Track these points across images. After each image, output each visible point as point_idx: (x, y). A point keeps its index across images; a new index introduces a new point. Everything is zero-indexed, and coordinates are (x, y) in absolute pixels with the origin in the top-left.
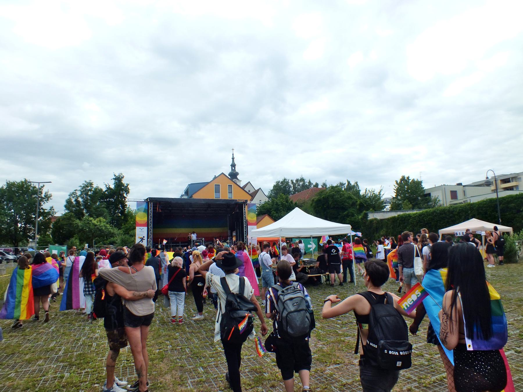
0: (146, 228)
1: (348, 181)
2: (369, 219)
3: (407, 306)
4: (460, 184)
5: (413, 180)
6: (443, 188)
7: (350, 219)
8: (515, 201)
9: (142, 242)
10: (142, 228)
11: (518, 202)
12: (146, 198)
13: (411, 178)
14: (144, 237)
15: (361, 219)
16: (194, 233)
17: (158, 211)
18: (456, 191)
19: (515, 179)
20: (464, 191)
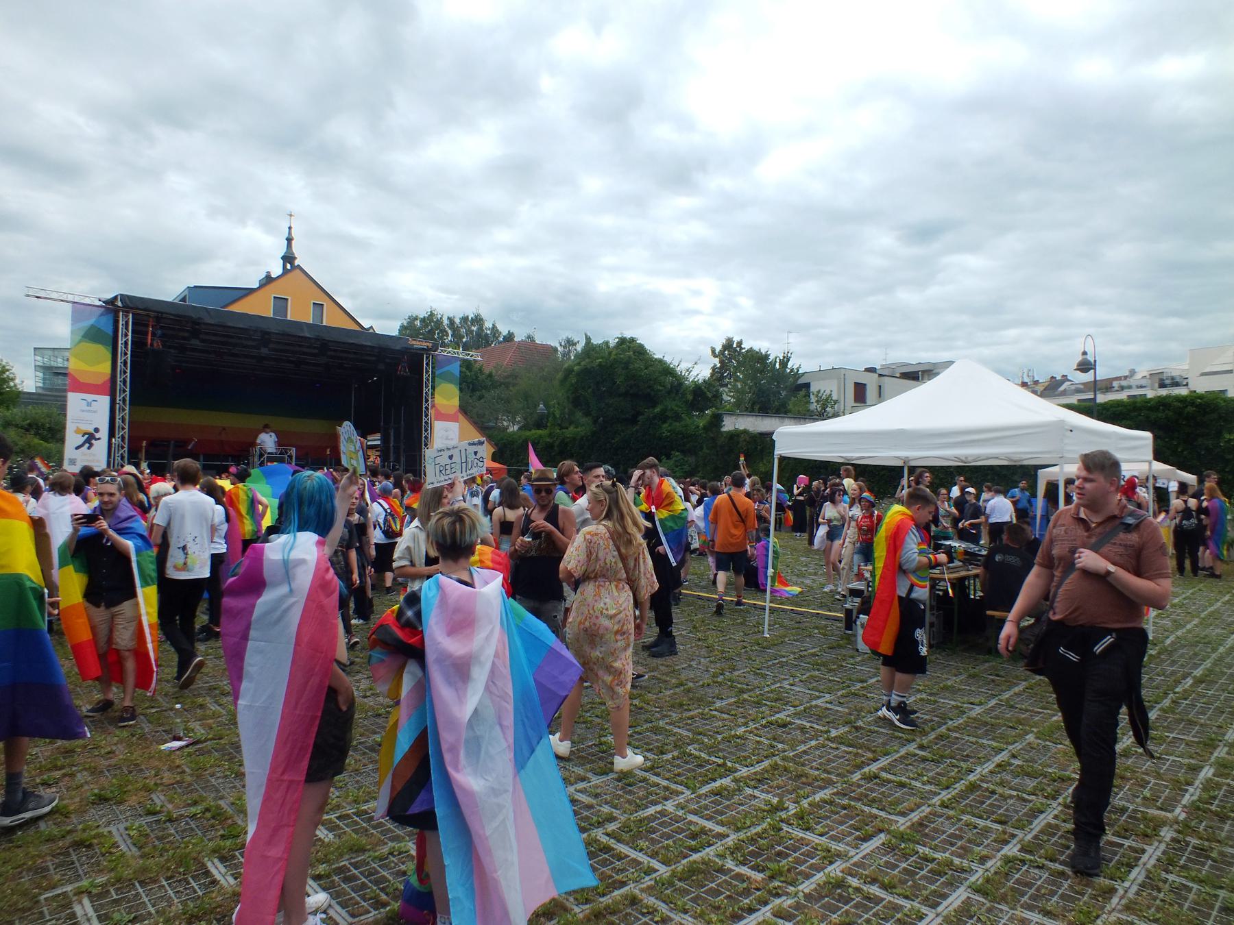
0: (105, 401)
1: (586, 335)
2: (724, 429)
4: (871, 370)
5: (751, 350)
6: (833, 373)
7: (669, 426)
8: (1133, 414)
9: (89, 448)
10: (90, 397)
11: (1140, 417)
12: (110, 296)
13: (746, 346)
14: (97, 430)
15: (705, 428)
16: (266, 428)
17: (152, 345)
18: (865, 384)
19: (929, 375)
20: (880, 386)
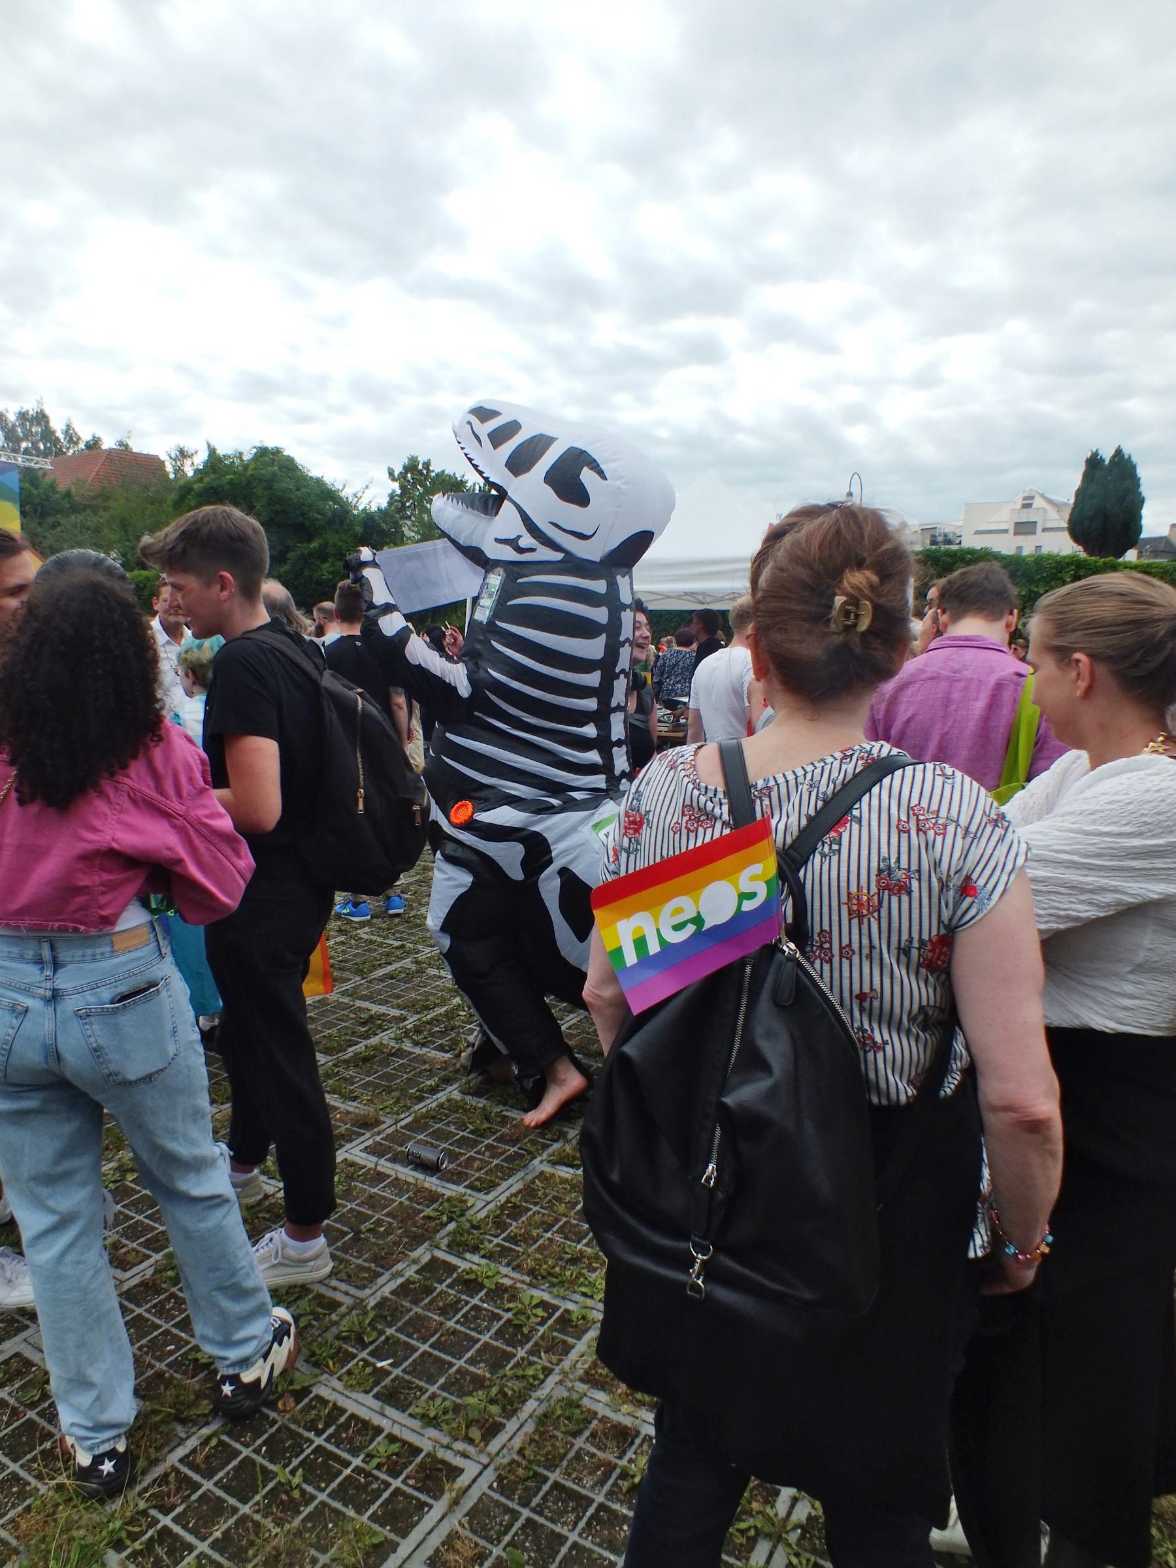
3: (640, 943)
